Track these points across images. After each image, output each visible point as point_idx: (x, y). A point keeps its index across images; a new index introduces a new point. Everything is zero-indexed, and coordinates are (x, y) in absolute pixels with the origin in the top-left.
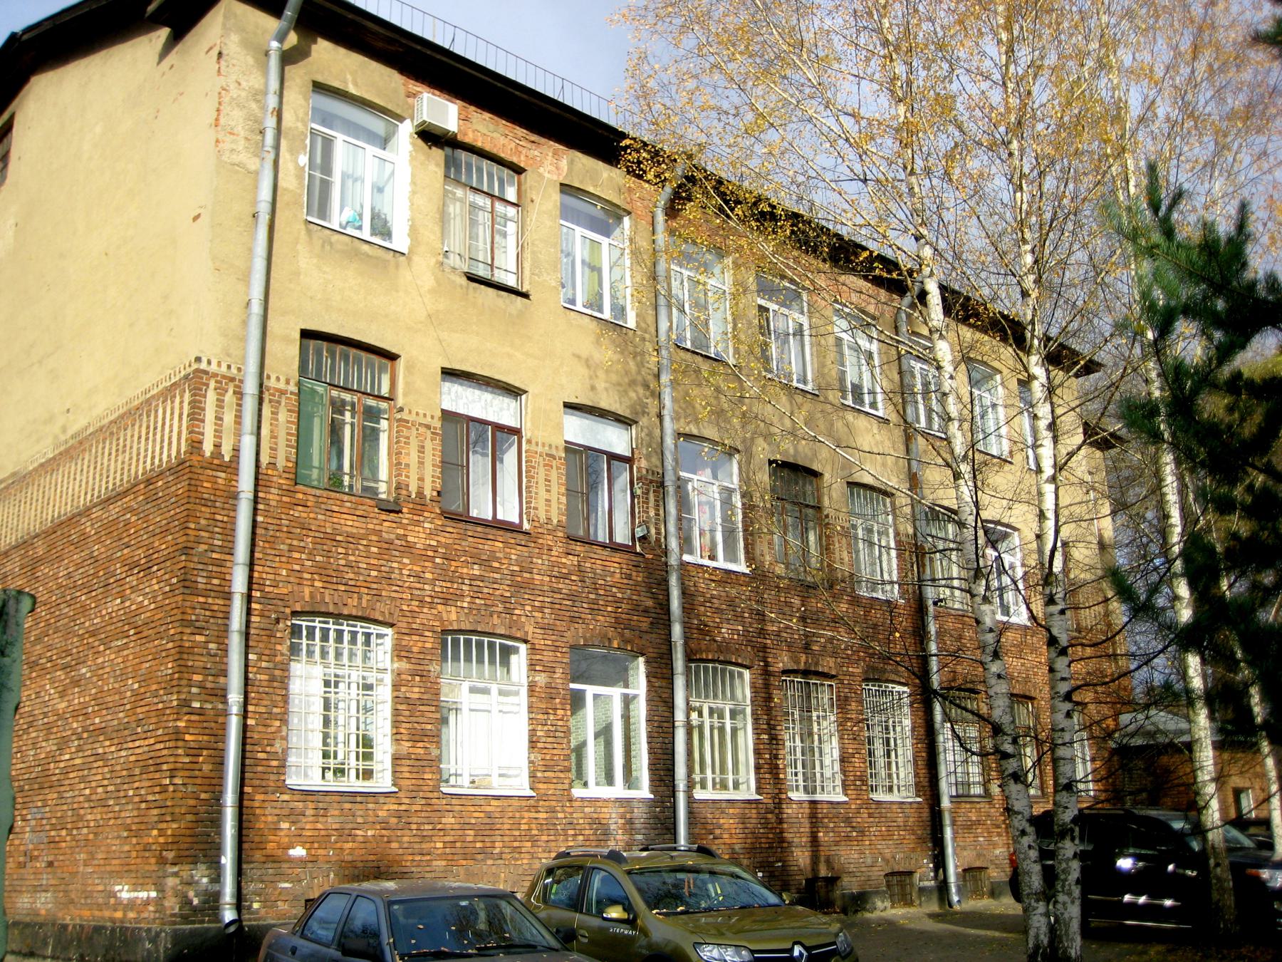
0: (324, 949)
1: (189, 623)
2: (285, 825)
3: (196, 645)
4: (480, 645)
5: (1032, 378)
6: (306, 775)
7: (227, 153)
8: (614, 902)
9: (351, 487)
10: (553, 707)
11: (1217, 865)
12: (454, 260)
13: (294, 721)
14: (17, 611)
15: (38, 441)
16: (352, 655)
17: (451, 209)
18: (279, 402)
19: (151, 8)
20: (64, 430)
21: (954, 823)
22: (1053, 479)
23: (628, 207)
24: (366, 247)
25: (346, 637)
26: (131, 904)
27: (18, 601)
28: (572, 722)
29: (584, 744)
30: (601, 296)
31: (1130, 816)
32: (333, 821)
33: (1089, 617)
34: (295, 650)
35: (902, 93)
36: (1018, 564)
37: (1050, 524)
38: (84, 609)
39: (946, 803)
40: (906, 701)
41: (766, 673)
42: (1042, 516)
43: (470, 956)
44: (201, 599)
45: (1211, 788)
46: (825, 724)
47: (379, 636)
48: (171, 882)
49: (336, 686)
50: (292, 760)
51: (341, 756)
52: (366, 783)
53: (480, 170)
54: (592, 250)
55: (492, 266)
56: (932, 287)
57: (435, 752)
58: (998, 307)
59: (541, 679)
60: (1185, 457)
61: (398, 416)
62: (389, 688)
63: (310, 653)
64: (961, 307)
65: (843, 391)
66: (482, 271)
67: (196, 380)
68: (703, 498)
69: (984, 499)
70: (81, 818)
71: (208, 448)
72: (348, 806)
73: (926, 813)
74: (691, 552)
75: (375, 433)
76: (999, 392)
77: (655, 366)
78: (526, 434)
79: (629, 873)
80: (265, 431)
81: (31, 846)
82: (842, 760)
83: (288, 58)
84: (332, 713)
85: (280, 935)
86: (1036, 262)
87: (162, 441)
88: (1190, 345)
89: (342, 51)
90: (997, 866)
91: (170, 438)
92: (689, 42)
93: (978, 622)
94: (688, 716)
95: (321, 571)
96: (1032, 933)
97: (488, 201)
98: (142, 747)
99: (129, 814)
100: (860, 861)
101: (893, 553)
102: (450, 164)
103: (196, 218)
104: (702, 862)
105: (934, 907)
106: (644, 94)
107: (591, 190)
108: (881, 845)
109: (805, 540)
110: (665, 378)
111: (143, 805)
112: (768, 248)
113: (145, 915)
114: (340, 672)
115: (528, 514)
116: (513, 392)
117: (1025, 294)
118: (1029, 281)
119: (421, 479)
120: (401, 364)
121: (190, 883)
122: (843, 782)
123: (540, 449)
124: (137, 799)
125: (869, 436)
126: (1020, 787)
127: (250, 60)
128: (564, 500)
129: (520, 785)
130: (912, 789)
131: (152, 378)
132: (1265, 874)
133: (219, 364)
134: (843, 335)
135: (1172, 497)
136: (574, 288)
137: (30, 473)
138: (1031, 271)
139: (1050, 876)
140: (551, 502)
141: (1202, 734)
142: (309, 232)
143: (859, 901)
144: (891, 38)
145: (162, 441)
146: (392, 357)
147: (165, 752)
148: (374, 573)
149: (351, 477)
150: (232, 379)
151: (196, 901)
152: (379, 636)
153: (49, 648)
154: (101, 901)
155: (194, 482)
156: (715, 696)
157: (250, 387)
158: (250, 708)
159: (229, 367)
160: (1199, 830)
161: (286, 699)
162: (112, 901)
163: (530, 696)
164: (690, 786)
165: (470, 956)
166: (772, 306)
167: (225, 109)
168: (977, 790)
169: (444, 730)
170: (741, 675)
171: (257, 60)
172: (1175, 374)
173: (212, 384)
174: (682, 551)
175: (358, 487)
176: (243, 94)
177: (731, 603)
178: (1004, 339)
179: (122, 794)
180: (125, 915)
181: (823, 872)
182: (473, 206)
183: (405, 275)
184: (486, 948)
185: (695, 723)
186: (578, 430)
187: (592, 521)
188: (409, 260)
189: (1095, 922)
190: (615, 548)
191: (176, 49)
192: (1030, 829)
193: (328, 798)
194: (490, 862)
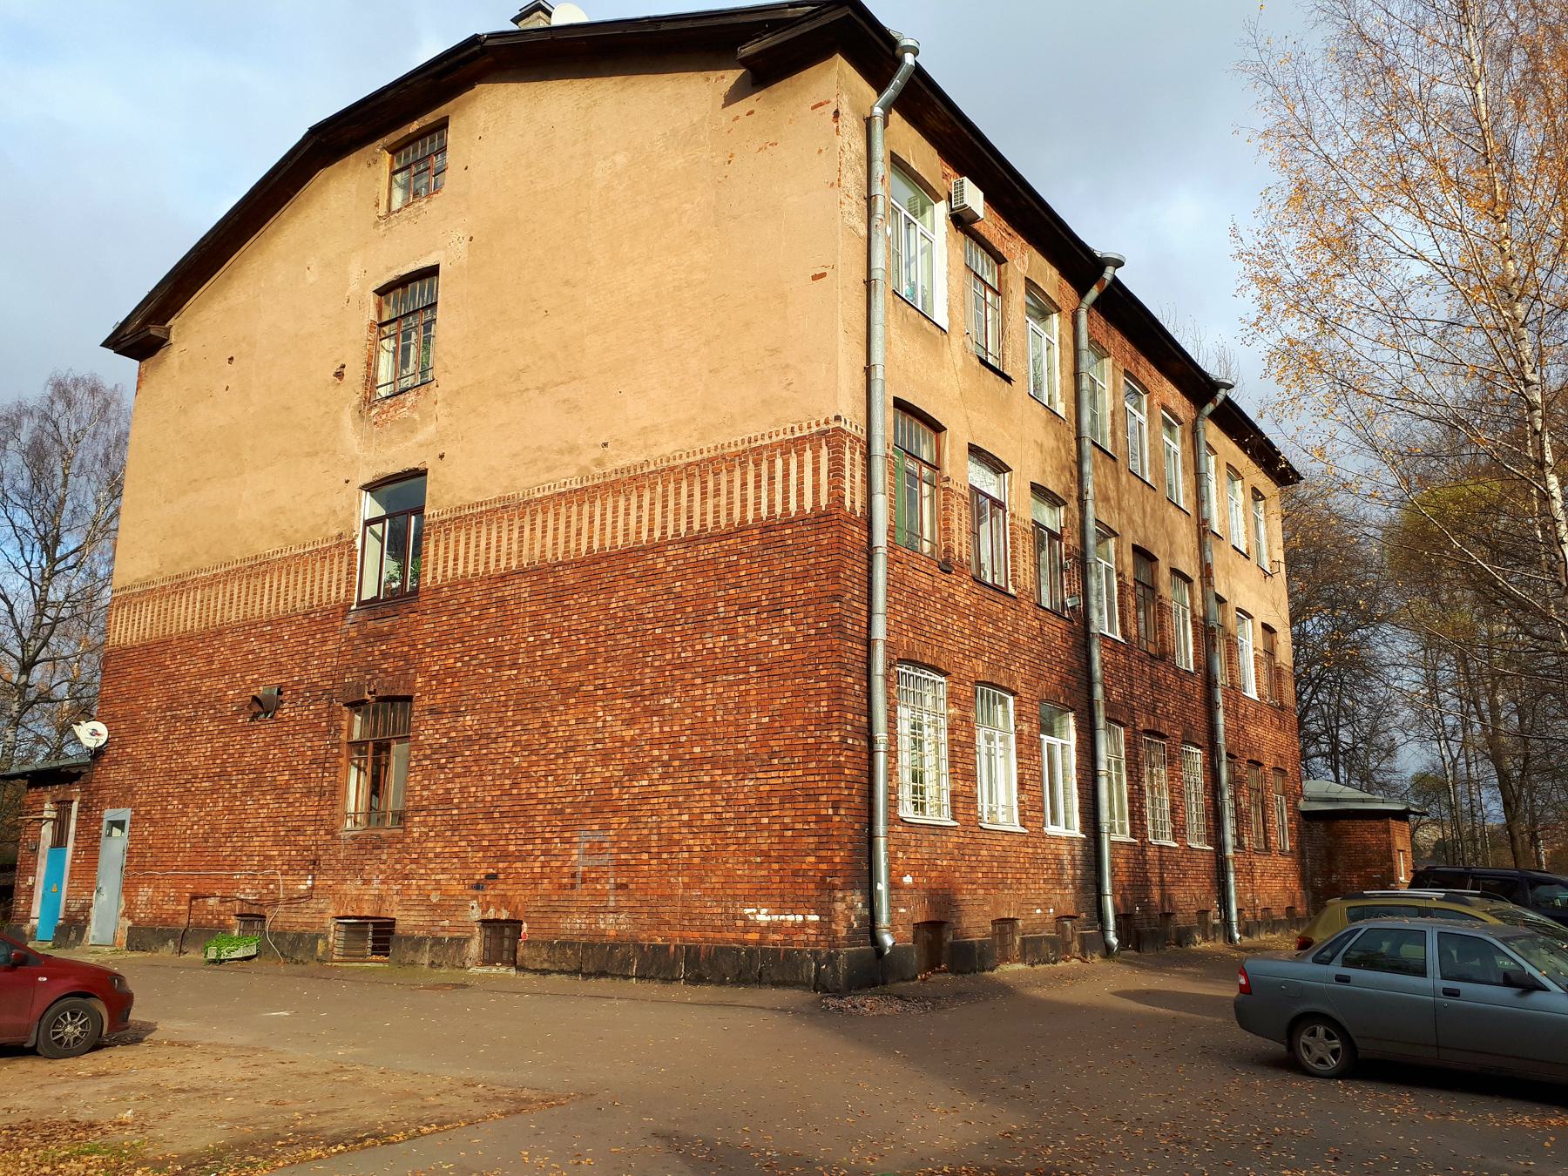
26: (772, 927)
59: (1025, 727)
61: (945, 485)
143: (1183, 937)
191: (756, 96)
193: (922, 830)
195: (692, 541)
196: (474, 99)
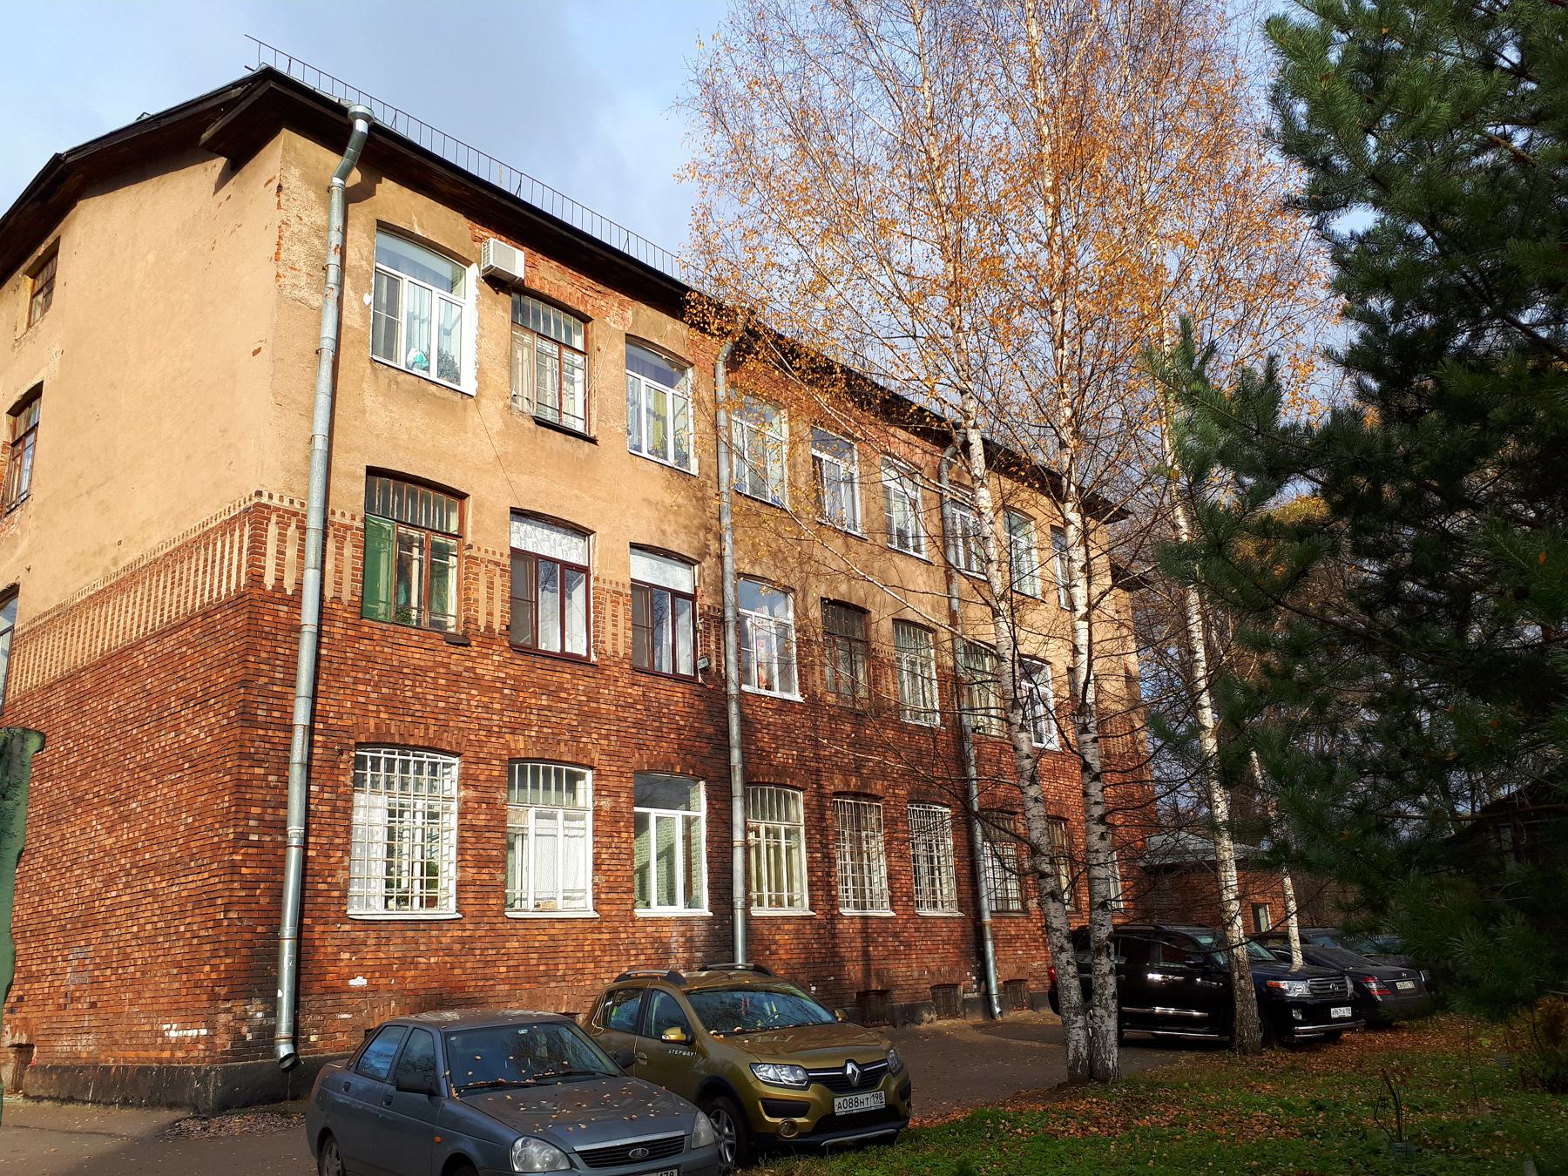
0: (379, 1085)
1: (249, 756)
2: (345, 956)
3: (255, 777)
4: (547, 772)
5: (1067, 522)
6: (368, 905)
7: (289, 289)
8: (672, 1024)
9: (418, 621)
10: (617, 831)
11: (1242, 977)
12: (522, 404)
13: (357, 851)
14: (22, 750)
15: (87, 573)
16: (418, 784)
17: (519, 355)
18: (344, 538)
19: (205, 136)
20: (115, 562)
21: (995, 937)
22: (1086, 617)
23: (690, 359)
24: (433, 388)
25: (412, 767)
26: (180, 1044)
27: (24, 740)
28: (636, 844)
29: (647, 865)
30: (664, 444)
31: (1159, 933)
32: (395, 950)
33: (1118, 745)
34: (358, 781)
35: (952, 249)
36: (1051, 694)
37: (1084, 658)
38: (136, 743)
39: (987, 918)
40: (948, 823)
41: (821, 796)
42: (1075, 651)
43: (527, 1086)
44: (261, 732)
45: (1235, 907)
46: (873, 843)
47: (446, 765)
48: (223, 1018)
49: (401, 816)
50: (354, 889)
51: (404, 884)
52: (430, 911)
53: (547, 319)
54: (656, 397)
55: (560, 411)
56: (975, 438)
57: (500, 877)
58: (1039, 458)
59: (606, 804)
60: (1214, 594)
61: (467, 553)
62: (455, 817)
63: (375, 784)
64: (1002, 460)
65: (888, 533)
66: (550, 416)
67: (257, 515)
68: (760, 633)
69: (1021, 635)
70: (127, 956)
71: (269, 581)
72: (410, 934)
73: (970, 929)
74: (748, 683)
75: (445, 568)
76: (1033, 538)
77: (716, 510)
78: (594, 572)
79: (687, 993)
80: (329, 566)
81: (72, 987)
82: (889, 877)
83: (352, 196)
84: (396, 844)
85: (334, 1071)
86: (1075, 414)
87: (221, 574)
88: (1222, 492)
89: (407, 191)
90: (1036, 978)
91: (229, 571)
92: (754, 198)
93: (1016, 749)
94: (746, 836)
95: (388, 703)
96: (1072, 1045)
97: (556, 348)
98: (194, 881)
99: (179, 951)
100: (910, 972)
101: (935, 684)
102: (517, 309)
103: (256, 352)
104: (757, 980)
105: (979, 1019)
106: (708, 250)
107: (656, 341)
108: (928, 959)
109: (854, 672)
110: (726, 521)
111: (195, 941)
112: (823, 399)
113: (195, 1054)
114: (404, 801)
115: (596, 647)
116: (582, 532)
117: (1063, 445)
118: (1066, 434)
119: (490, 614)
120: (470, 504)
121: (244, 1018)
122: (891, 898)
123: (607, 586)
124: (188, 935)
125: (920, 579)
126: (1057, 905)
127: (312, 196)
128: (630, 633)
129: (584, 907)
130: (955, 904)
131: (211, 511)
132: (1284, 985)
133: (281, 498)
134: (892, 484)
135: (1197, 634)
136: (640, 433)
137: (78, 605)
138: (1069, 423)
139: (1087, 990)
140: (618, 636)
141: (1227, 855)
142: (374, 369)
143: (911, 1013)
144: (943, 199)
145: (221, 574)
146: (462, 496)
147: (220, 886)
148: (442, 704)
149: (419, 611)
150: (295, 514)
151: (249, 1037)
152: (446, 765)
153: (96, 783)
154: (147, 1041)
155: (257, 614)
156: (771, 818)
157: (314, 521)
158: (312, 840)
159: (292, 502)
160: (1225, 945)
161: (348, 829)
162: (159, 1040)
163: (595, 820)
164: (748, 903)
165: (527, 1086)
166: (825, 457)
167: (285, 244)
168: (1016, 906)
169: (510, 855)
170: (795, 797)
171: (318, 196)
172: (1206, 517)
173: (274, 518)
174: (741, 682)
175: (425, 621)
176: (305, 229)
177: (787, 729)
178: (1042, 490)
179: (173, 930)
180: (173, 1055)
181: (875, 986)
182: (541, 352)
183: (474, 418)
184: (544, 1077)
185: (753, 843)
186: (645, 569)
187: (657, 654)
188: (477, 402)
189: (1129, 1033)
190: (676, 677)
192: (1068, 946)
193: (390, 927)
194: (553, 985)
195: (160, 635)
196: (74, 217)
